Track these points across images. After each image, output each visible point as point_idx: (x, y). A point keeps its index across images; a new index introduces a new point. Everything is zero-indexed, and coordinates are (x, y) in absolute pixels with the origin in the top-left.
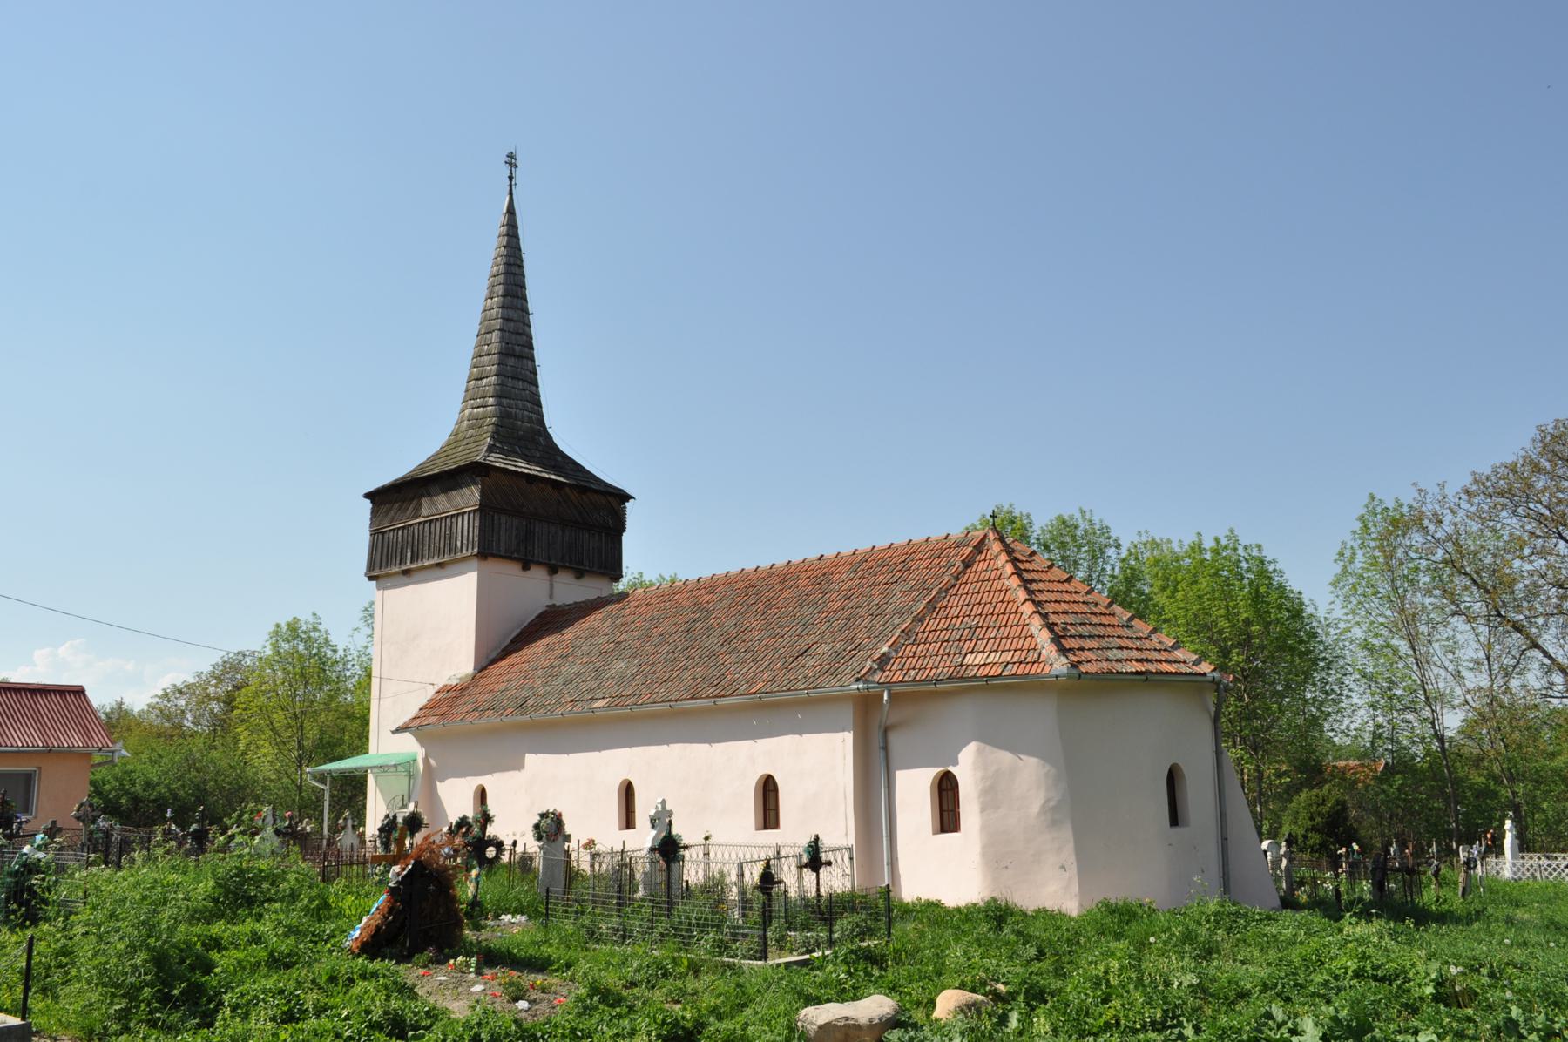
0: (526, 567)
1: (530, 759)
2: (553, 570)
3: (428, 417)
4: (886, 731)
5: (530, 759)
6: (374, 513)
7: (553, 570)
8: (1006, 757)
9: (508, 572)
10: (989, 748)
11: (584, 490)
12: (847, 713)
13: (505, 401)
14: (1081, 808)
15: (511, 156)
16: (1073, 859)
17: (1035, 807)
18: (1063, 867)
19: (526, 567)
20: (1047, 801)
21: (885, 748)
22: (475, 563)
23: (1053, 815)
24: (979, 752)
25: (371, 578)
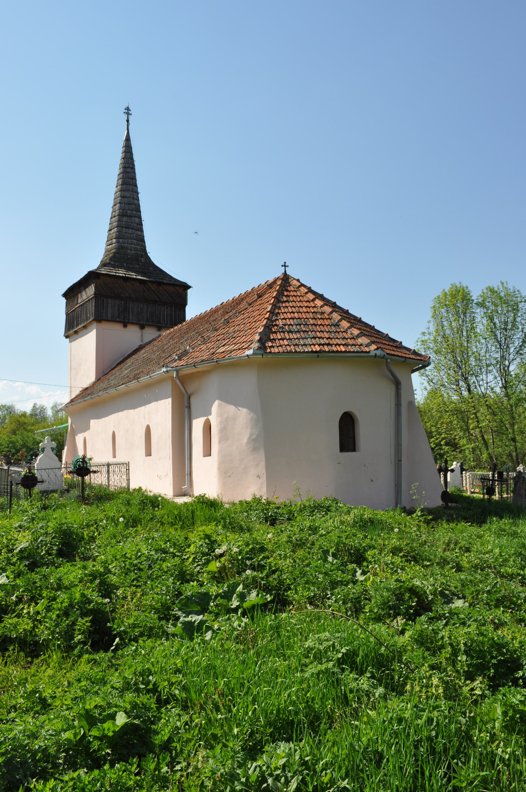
0: (125, 326)
1: (93, 422)
2: (142, 327)
3: (91, 253)
4: (189, 398)
5: (93, 422)
6: (67, 303)
7: (142, 327)
8: (231, 408)
9: (115, 330)
10: (224, 403)
11: (160, 284)
12: (168, 387)
13: (121, 240)
14: (272, 440)
15: (128, 109)
16: (264, 471)
17: (245, 440)
18: (258, 476)
19: (125, 326)
20: (251, 435)
21: (189, 407)
22: (95, 324)
23: (255, 444)
24: (219, 406)
25: (67, 337)
